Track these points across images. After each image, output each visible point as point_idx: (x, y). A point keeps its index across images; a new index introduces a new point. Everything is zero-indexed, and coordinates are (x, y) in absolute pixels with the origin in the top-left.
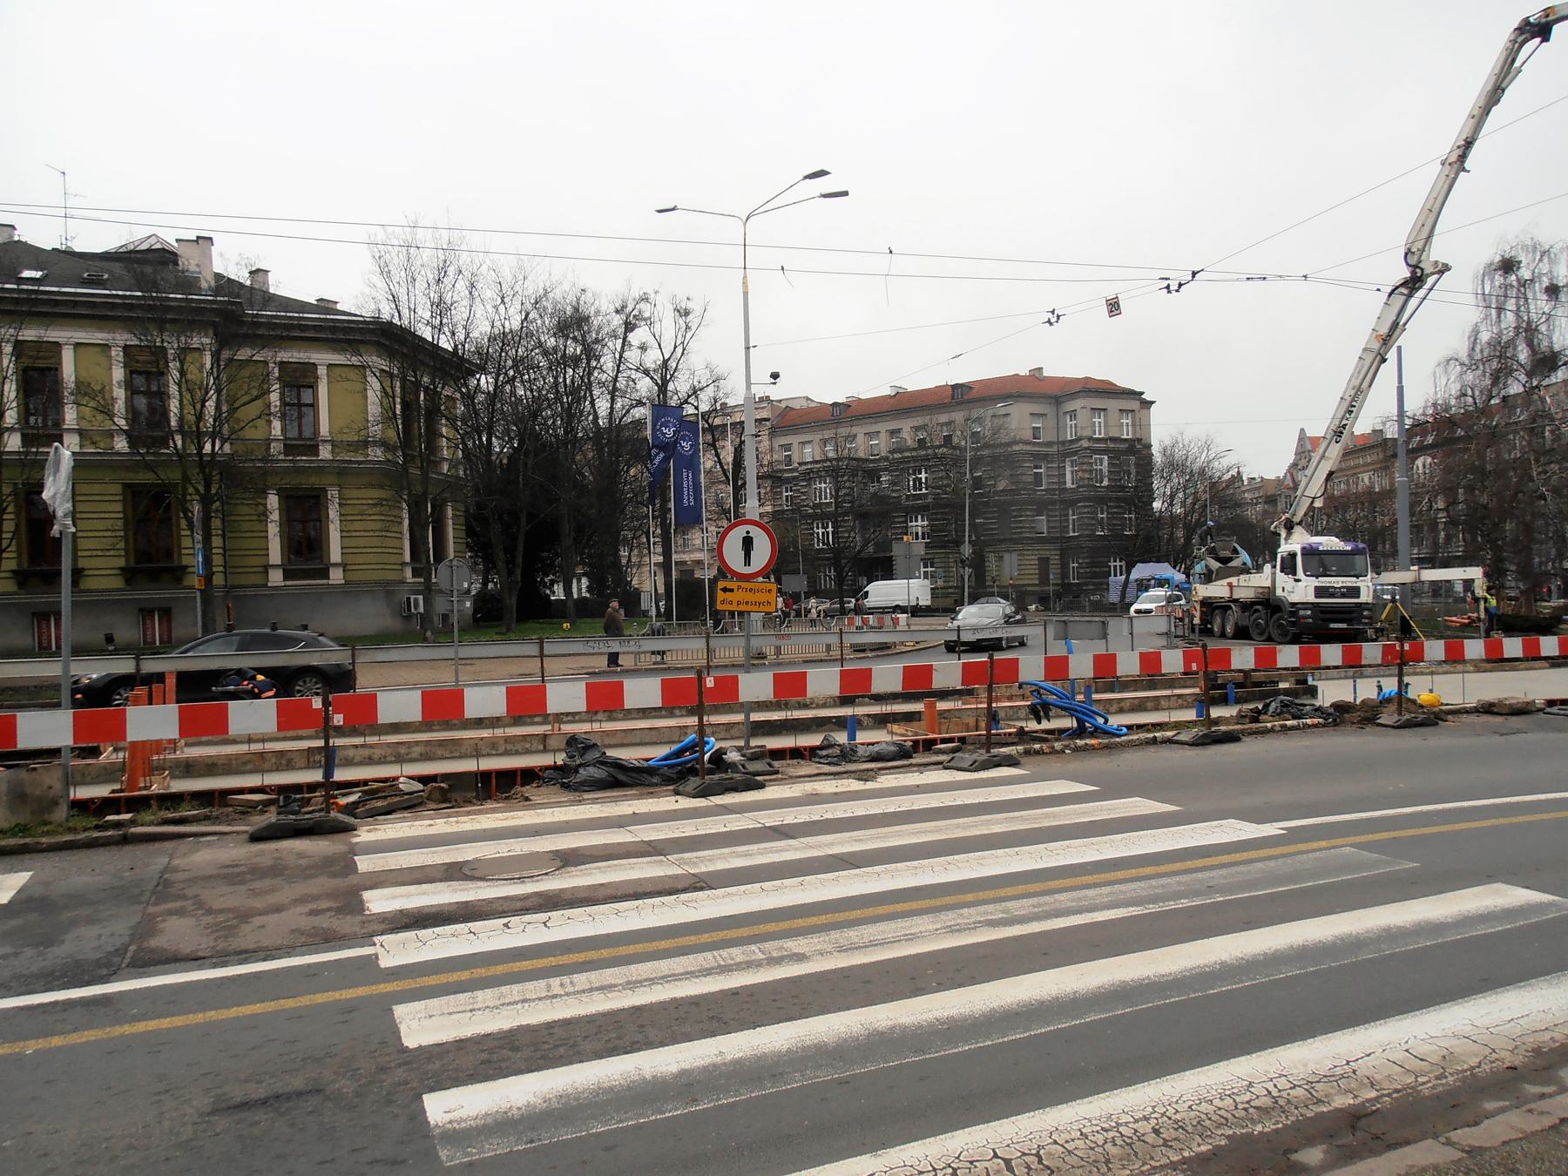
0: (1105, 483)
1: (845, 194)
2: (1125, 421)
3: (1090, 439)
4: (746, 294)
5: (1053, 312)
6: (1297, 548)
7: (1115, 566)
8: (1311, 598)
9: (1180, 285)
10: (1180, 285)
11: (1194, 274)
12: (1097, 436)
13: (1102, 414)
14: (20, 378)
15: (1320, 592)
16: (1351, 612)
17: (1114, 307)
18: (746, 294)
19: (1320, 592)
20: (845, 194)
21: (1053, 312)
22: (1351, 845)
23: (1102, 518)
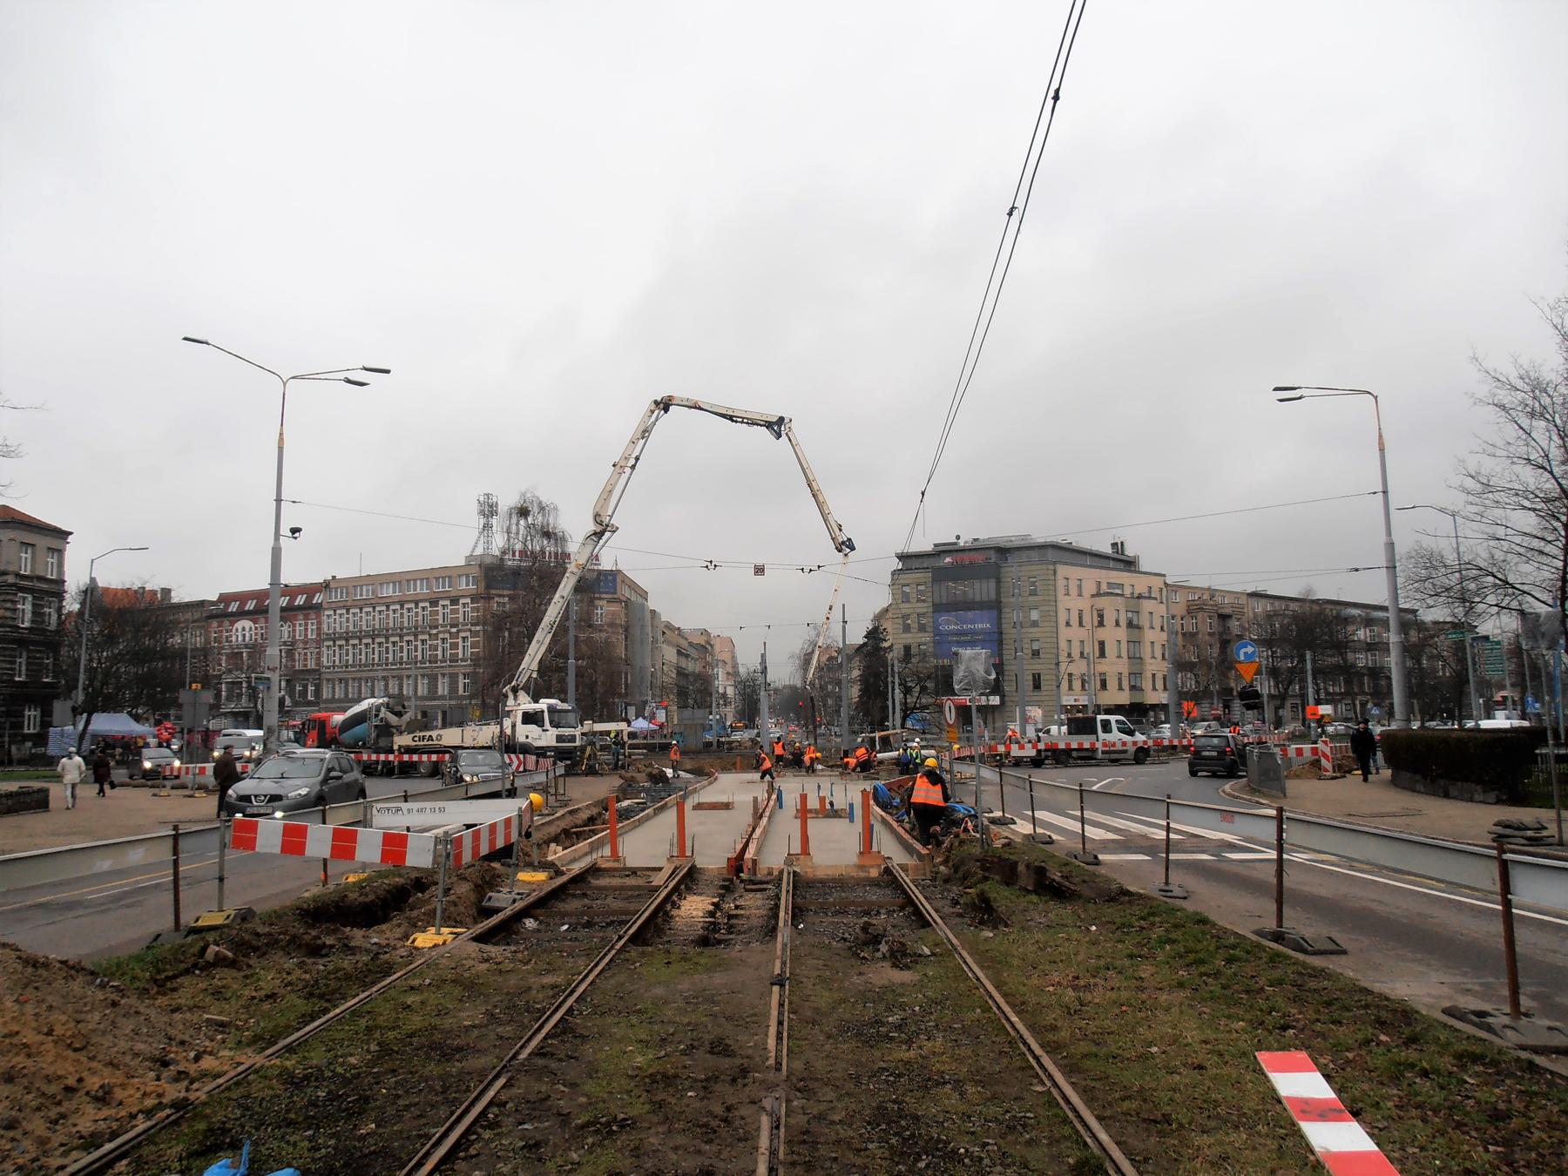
0: (26, 625)
1: (387, 372)
2: (23, 555)
3: (18, 575)
4: (281, 449)
5: (711, 562)
6: (544, 707)
7: (29, 716)
8: (554, 743)
9: (811, 570)
10: (811, 570)
11: (819, 567)
12: (22, 572)
13: (29, 551)
14: (1454, 735)
15: (560, 738)
16: (571, 753)
17: (759, 570)
18: (281, 449)
19: (560, 738)
20: (387, 372)
21: (711, 562)
22: (1522, 837)
23: (48, 664)
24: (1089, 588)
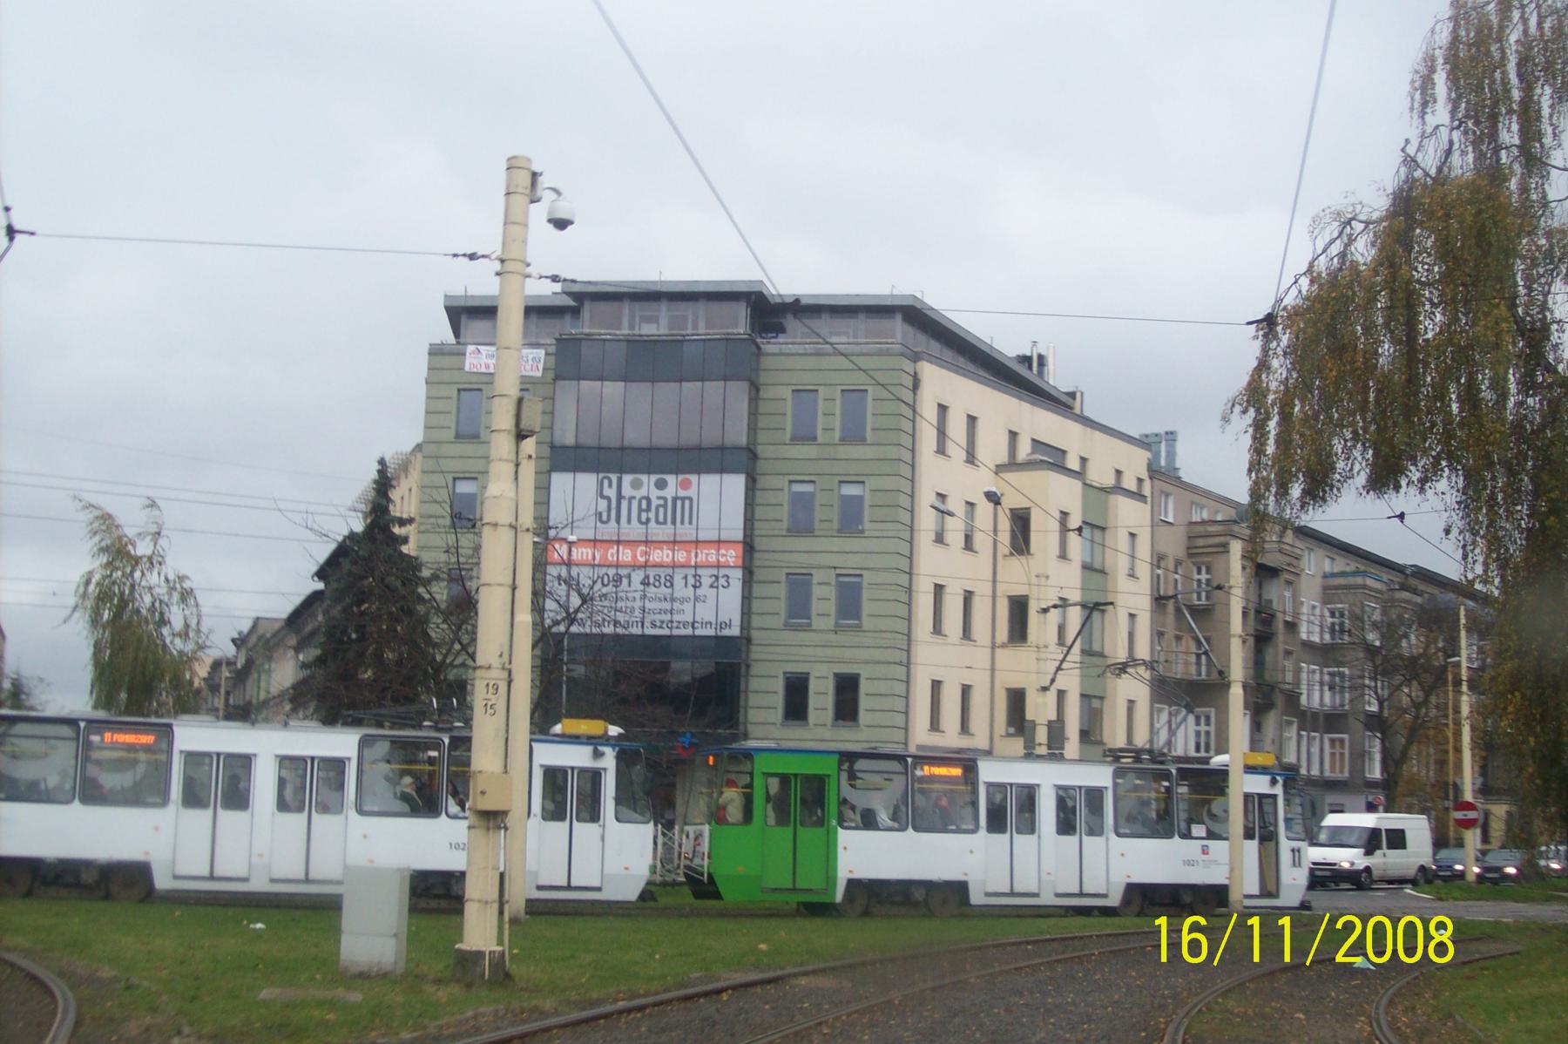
24: (992, 448)
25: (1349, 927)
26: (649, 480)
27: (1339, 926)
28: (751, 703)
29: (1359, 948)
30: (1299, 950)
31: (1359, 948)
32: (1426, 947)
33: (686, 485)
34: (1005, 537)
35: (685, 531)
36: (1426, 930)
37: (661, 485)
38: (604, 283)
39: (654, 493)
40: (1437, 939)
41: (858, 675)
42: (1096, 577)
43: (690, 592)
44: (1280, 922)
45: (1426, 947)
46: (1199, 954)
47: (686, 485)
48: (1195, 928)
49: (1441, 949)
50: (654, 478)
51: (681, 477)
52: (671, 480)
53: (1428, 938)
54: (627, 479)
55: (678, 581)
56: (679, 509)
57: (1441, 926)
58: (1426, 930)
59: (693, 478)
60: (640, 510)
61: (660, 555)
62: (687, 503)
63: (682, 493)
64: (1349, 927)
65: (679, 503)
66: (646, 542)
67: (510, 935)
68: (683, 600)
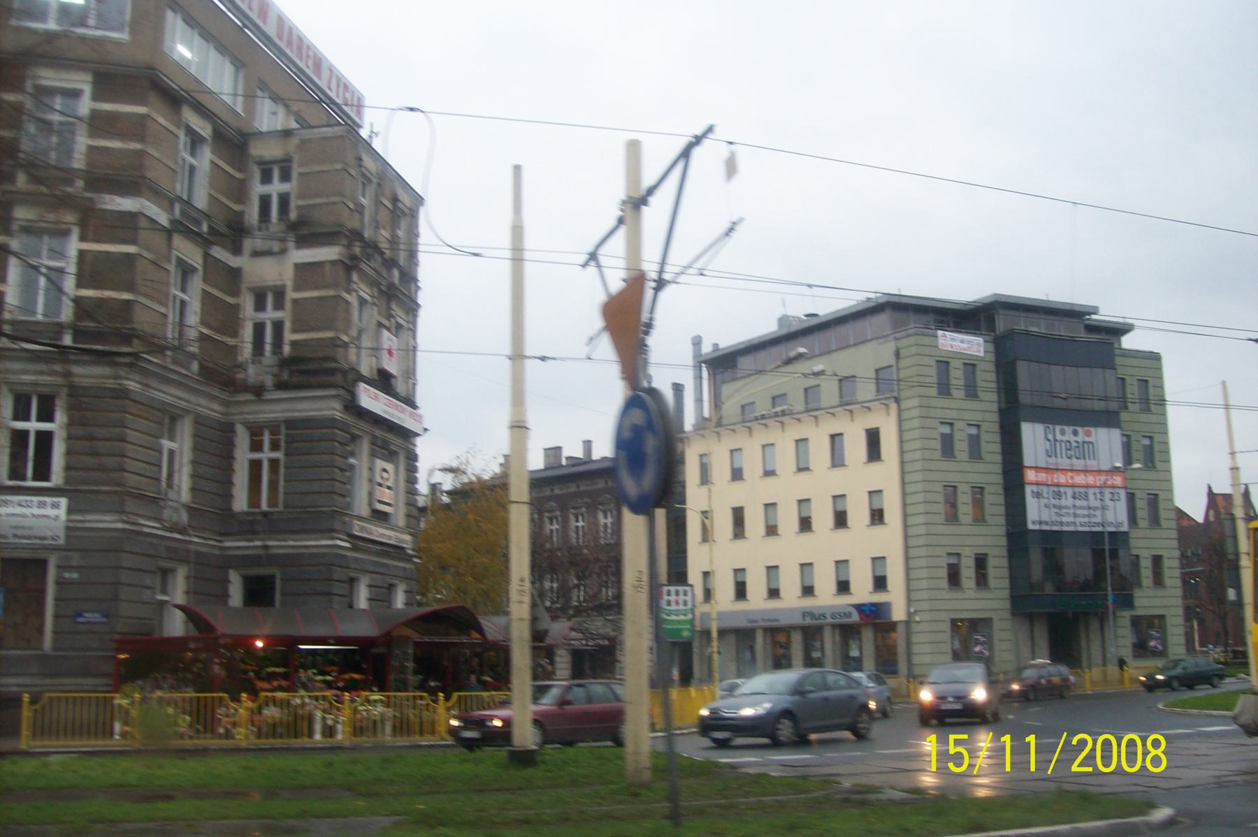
25: (1083, 743)
26: (1069, 429)
27: (1074, 742)
28: (1007, 580)
29: (1090, 759)
30: (1043, 763)
31: (1090, 759)
32: (1144, 760)
33: (1088, 434)
34: (177, 458)
35: (1092, 464)
36: (1144, 745)
37: (1075, 433)
38: (933, 299)
39: (1073, 438)
40: (1153, 752)
41: (986, 555)
42: (1235, 471)
43: (1098, 504)
44: (1027, 739)
45: (1144, 760)
46: (962, 765)
47: (1088, 434)
48: (957, 742)
49: (1156, 761)
50: (1072, 428)
51: (1086, 428)
52: (1080, 430)
53: (1145, 753)
54: (1058, 428)
55: (1091, 497)
56: (1086, 450)
57: (1156, 744)
58: (1144, 745)
59: (1092, 430)
60: (1067, 449)
61: (1080, 479)
62: (1091, 446)
63: (1087, 439)
64: (1083, 743)
65: (1086, 445)
66: (1072, 471)
67: (1057, 748)
68: (1095, 509)
